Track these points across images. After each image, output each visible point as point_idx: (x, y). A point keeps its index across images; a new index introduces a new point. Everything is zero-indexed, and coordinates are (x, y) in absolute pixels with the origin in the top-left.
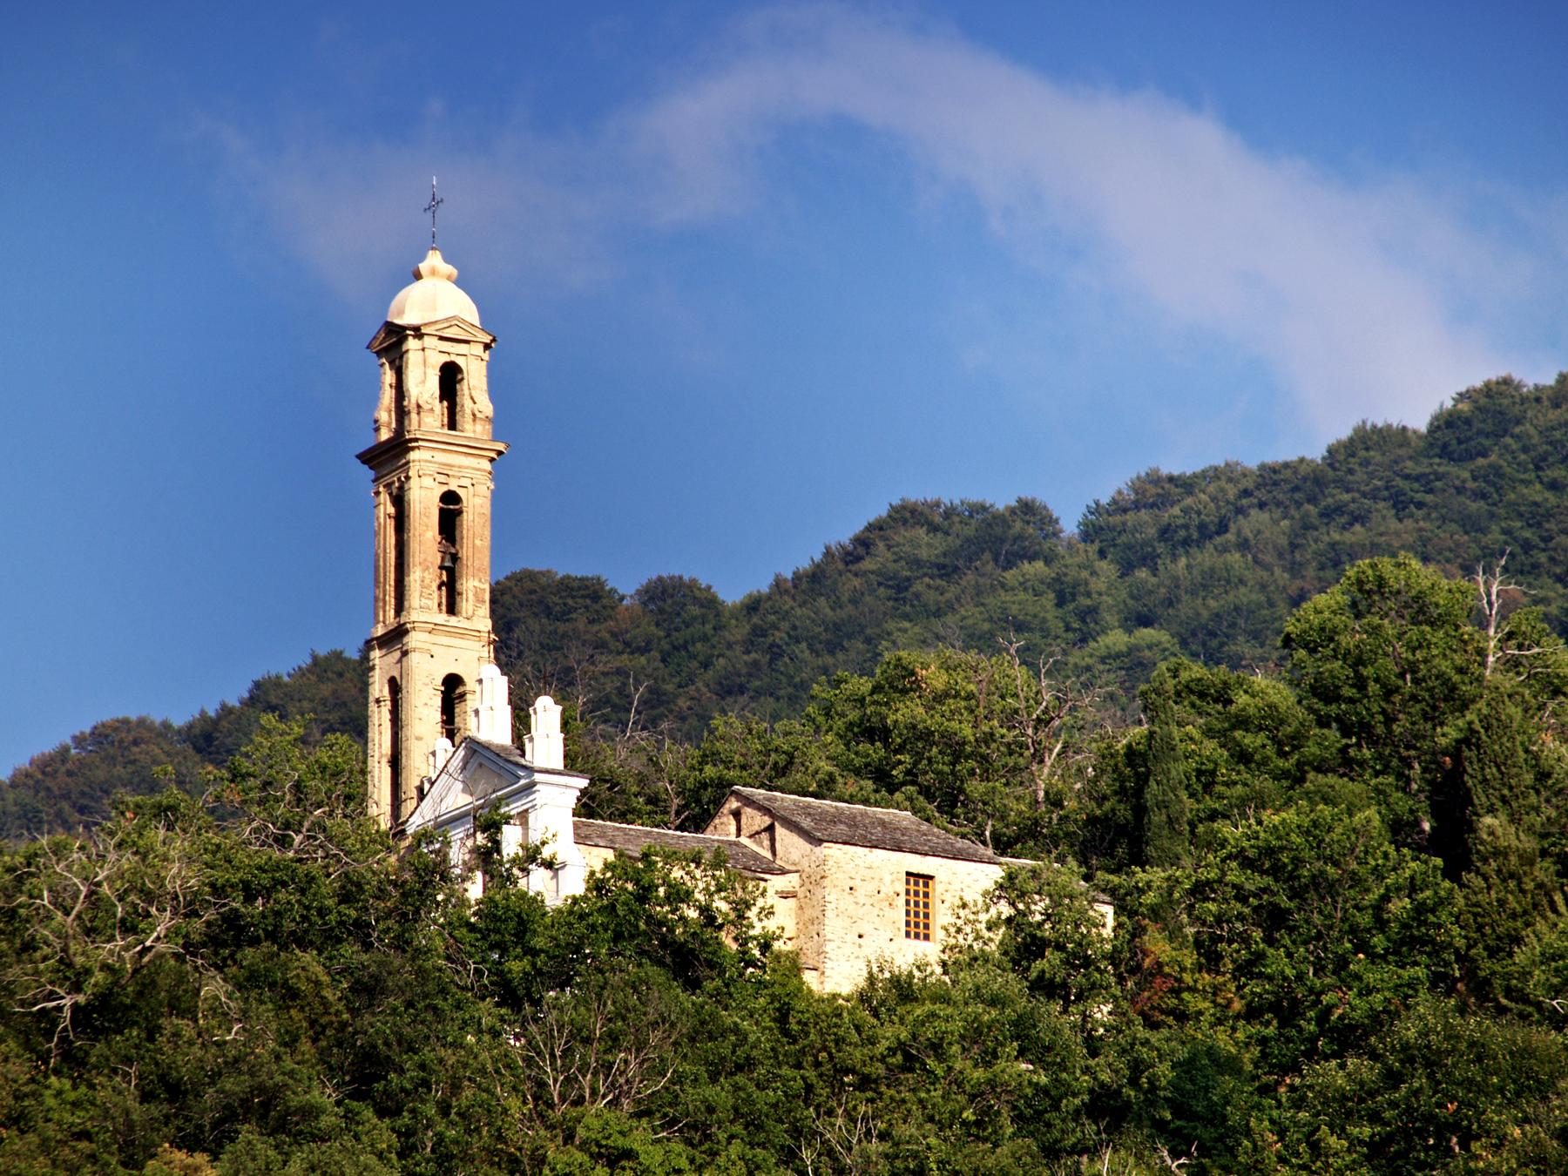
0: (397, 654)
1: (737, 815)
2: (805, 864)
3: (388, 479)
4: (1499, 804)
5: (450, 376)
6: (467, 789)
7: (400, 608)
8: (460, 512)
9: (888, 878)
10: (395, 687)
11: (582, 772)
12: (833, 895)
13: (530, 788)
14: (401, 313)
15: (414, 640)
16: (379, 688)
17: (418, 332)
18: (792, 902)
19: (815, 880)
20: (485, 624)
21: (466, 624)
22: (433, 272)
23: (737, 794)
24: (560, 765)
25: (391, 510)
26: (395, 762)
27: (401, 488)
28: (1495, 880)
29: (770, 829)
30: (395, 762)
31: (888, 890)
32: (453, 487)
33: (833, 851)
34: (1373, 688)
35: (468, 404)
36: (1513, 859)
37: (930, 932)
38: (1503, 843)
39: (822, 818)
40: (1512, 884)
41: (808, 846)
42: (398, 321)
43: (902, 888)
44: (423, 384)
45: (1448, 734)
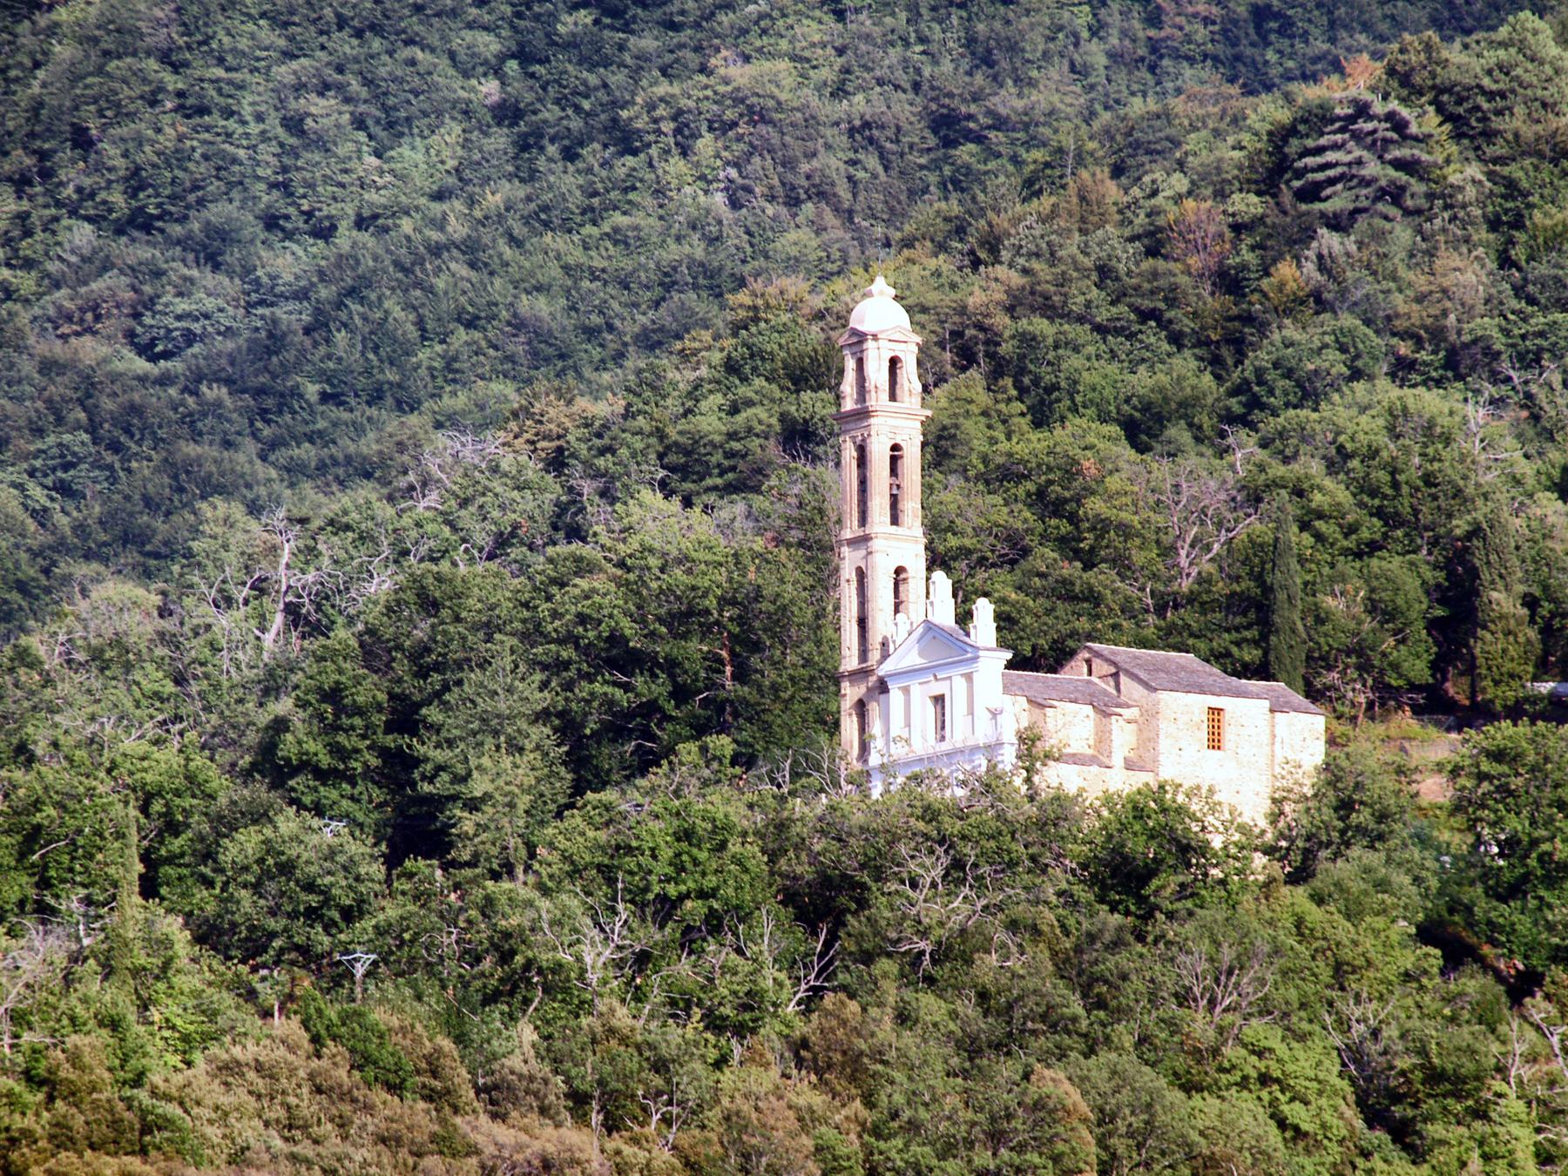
0: (863, 552)
1: (1089, 662)
2: (1143, 701)
3: (853, 433)
4: (1498, 579)
5: (894, 362)
6: (921, 654)
7: (863, 521)
8: (901, 457)
9: (1197, 711)
10: (861, 574)
11: (1008, 647)
12: (1164, 726)
13: (975, 659)
14: (861, 322)
15: (875, 544)
16: (848, 572)
17: (875, 337)
18: (1133, 726)
19: (1150, 716)
20: (918, 531)
21: (907, 532)
22: (881, 293)
23: (1089, 649)
24: (993, 644)
25: (855, 454)
26: (862, 623)
27: (864, 440)
28: (1500, 635)
29: (1115, 676)
30: (862, 623)
31: (1196, 719)
32: (898, 441)
33: (1164, 696)
34: (1405, 490)
35: (906, 384)
36: (1512, 622)
37: (888, 453)
38: (1505, 610)
39: (1156, 669)
40: (1511, 638)
41: (1146, 692)
42: (860, 328)
43: (1205, 718)
44: (877, 373)
45: (1460, 526)
